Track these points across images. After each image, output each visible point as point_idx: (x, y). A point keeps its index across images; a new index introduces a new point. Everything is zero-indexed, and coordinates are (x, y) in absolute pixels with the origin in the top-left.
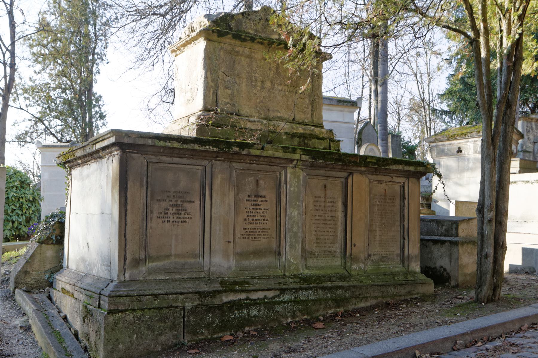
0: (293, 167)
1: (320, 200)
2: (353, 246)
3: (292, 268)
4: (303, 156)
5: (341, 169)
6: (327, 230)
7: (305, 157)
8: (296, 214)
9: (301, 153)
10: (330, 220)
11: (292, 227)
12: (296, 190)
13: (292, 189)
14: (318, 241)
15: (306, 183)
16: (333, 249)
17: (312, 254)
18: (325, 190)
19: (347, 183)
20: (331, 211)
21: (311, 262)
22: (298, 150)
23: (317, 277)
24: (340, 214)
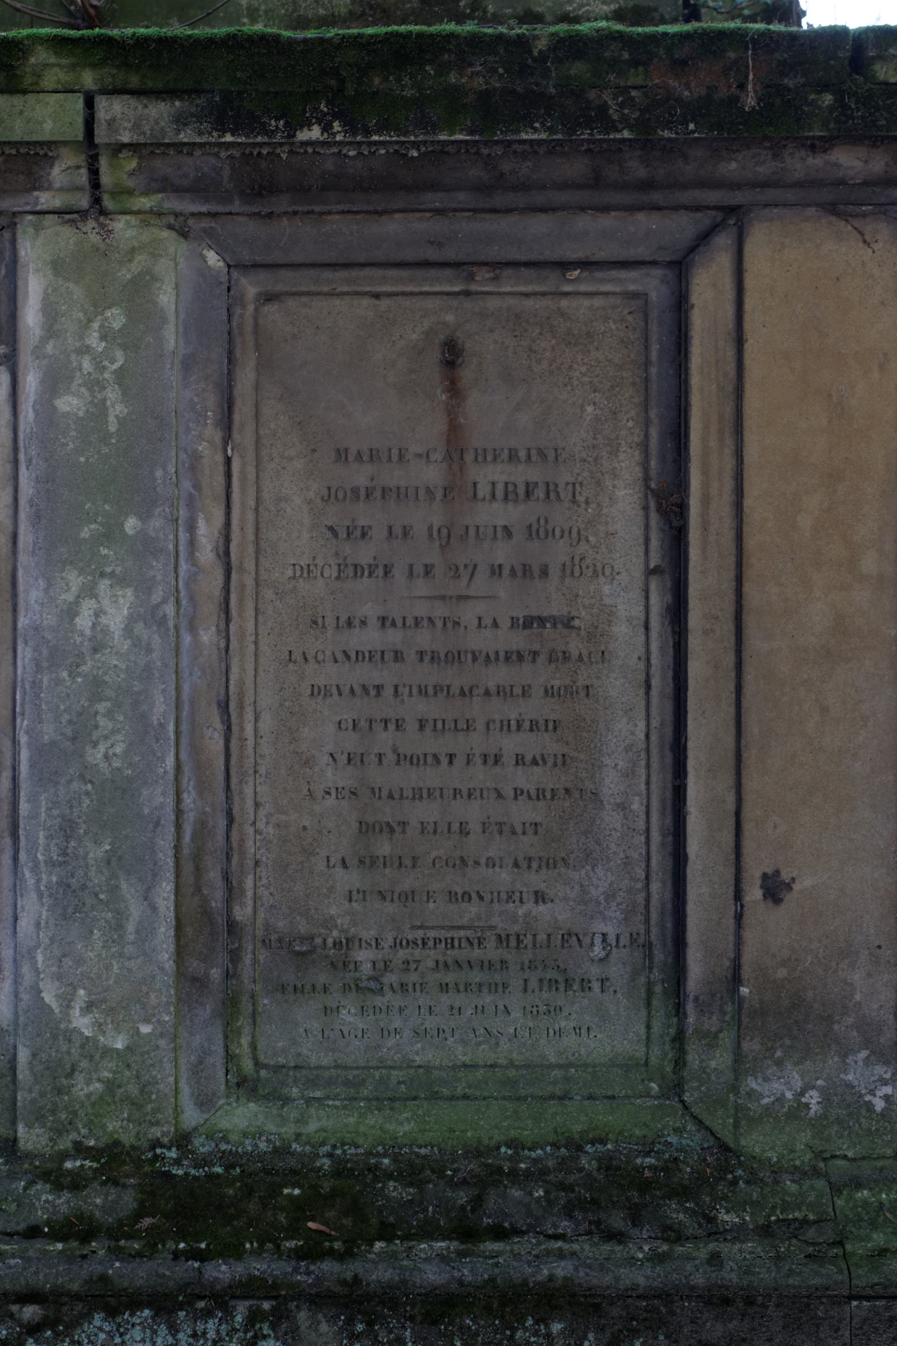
0: (68, 214)
1: (393, 477)
2: (754, 893)
3: (85, 1088)
4: (109, 109)
5: (597, 182)
6: (476, 741)
7: (120, 116)
8: (116, 619)
9: (88, 79)
10: (515, 657)
11: (81, 732)
12: (117, 409)
13: (68, 404)
14: (384, 848)
15: (225, 344)
16: (557, 914)
17: (312, 960)
18: (454, 390)
19: (681, 305)
20: (526, 572)
21: (296, 1033)
22: (41, 56)
23: (341, 1170)
24: (623, 600)
